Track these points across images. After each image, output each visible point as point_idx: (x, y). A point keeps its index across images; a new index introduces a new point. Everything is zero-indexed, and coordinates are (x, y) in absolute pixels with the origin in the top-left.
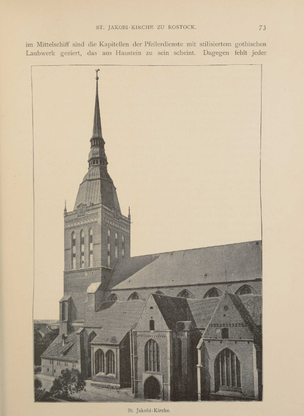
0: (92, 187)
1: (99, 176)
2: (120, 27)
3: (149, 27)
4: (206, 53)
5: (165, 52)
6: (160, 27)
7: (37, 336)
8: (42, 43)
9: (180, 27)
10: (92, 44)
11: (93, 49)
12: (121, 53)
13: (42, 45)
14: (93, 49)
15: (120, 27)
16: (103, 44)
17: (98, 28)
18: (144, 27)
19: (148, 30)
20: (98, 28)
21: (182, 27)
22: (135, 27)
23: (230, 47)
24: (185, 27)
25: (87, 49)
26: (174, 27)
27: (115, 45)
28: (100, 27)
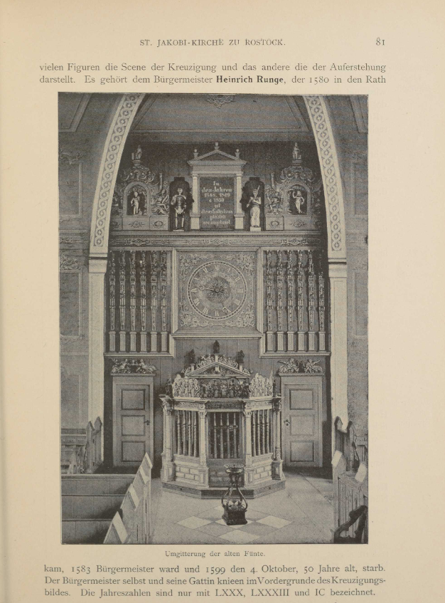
0: (280, 285)
1: (331, 267)
2: (176, 43)
6: (233, 42)
7: (363, 527)
9: (261, 42)
10: (299, 67)
11: (300, 74)
14: (300, 74)
15: (176, 43)
16: (174, 67)
18: (209, 43)
19: (215, 46)
22: (197, 43)
24: (269, 42)
25: (293, 73)
26: (253, 42)
27: (360, 68)
28: (145, 42)
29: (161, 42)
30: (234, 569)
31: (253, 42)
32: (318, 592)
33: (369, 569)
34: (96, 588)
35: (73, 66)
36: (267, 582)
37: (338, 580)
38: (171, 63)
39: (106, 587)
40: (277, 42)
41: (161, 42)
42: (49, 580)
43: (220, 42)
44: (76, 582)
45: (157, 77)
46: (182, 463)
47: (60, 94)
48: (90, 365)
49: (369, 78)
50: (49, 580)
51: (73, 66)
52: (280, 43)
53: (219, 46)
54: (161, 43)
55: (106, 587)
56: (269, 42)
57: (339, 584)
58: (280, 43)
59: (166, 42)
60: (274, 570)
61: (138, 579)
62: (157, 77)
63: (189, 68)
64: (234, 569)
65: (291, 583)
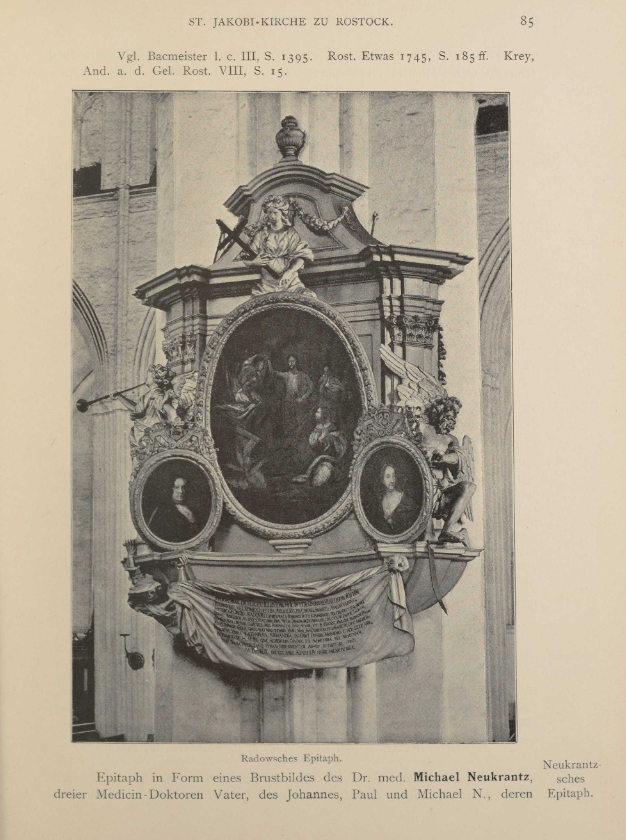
2: (239, 22)
3: (299, 22)
5: (135, 792)
6: (320, 21)
9: (359, 22)
13: (428, 795)
15: (239, 22)
17: (523, 20)
18: (286, 22)
21: (364, 22)
24: (370, 22)
26: (348, 22)
28: (196, 22)
29: (218, 21)
30: (328, 778)
31: (348, 22)
32: (159, 779)
33: (121, 779)
34: (281, 789)
36: (184, 779)
39: (295, 787)
40: (381, 22)
41: (218, 21)
42: (358, 777)
43: (301, 22)
45: (255, 775)
46: (111, 387)
50: (358, 777)
52: (384, 22)
53: (298, 27)
54: (218, 23)
55: (295, 787)
58: (384, 22)
60: (173, 796)
62: (255, 775)
64: (328, 778)
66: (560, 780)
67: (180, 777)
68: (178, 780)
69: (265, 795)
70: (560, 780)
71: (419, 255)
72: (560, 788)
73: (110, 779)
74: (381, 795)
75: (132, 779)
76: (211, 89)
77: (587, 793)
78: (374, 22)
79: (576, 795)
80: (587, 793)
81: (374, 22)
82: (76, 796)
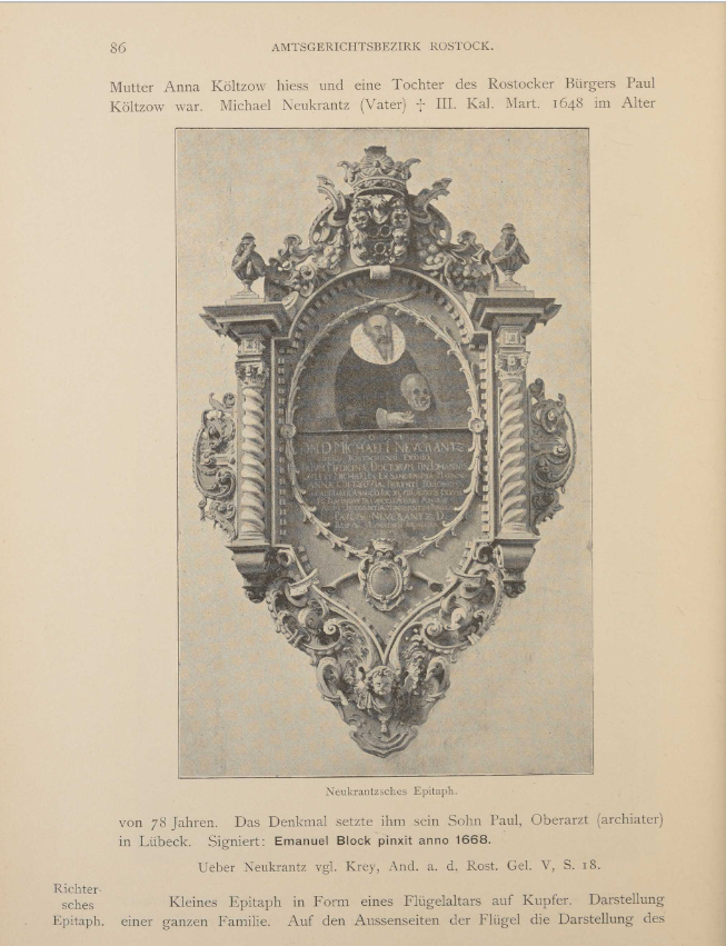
4: (275, 821)
8: (233, 102)
9: (456, 46)
12: (518, 105)
16: (476, 103)
19: (352, 52)
20: (115, 48)
23: (301, 907)
24: (467, 46)
26: (443, 46)
31: (443, 46)
32: (299, 903)
33: (461, 902)
35: (227, 920)
36: (327, 903)
37: (120, 106)
38: (217, 79)
40: (480, 46)
44: (588, 84)
47: (587, 763)
48: (425, 783)
49: (493, 81)
51: (227, 920)
52: (484, 47)
56: (467, 46)
57: (356, 873)
58: (484, 47)
59: (280, 46)
61: (396, 789)
63: (390, 46)
64: (388, 822)
65: (169, 925)
66: (66, 906)
67: (323, 901)
68: (487, 923)
69: (330, 921)
70: (66, 906)
71: (521, 306)
72: (67, 914)
73: (244, 903)
74: (525, 919)
75: (547, 901)
76: (592, 161)
77: (96, 921)
78: (472, 46)
79: (86, 923)
80: (96, 921)
81: (472, 46)
82: (287, 47)
